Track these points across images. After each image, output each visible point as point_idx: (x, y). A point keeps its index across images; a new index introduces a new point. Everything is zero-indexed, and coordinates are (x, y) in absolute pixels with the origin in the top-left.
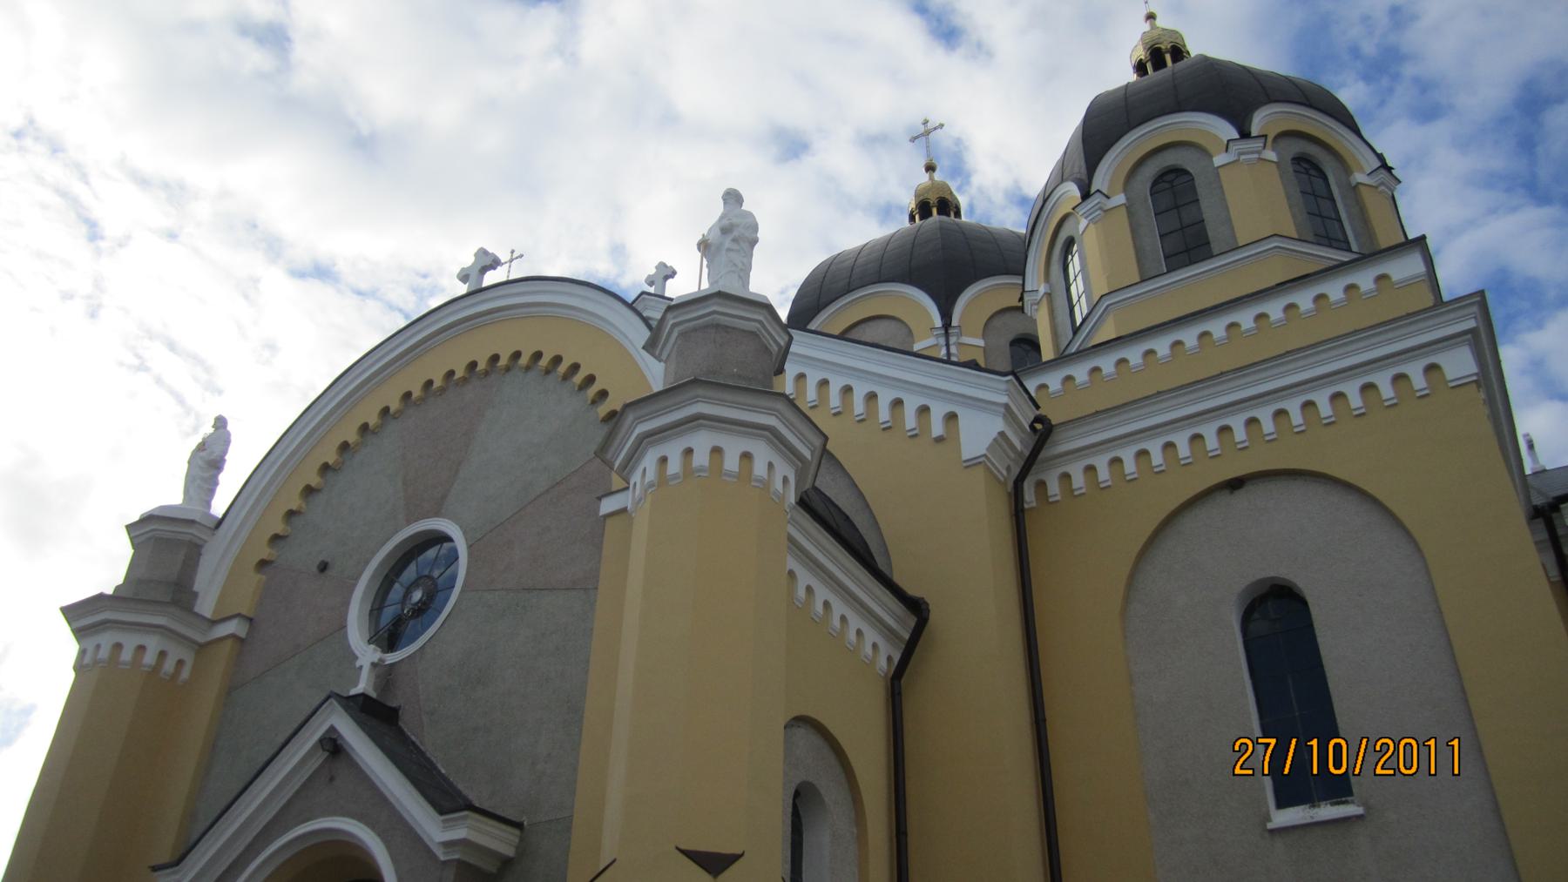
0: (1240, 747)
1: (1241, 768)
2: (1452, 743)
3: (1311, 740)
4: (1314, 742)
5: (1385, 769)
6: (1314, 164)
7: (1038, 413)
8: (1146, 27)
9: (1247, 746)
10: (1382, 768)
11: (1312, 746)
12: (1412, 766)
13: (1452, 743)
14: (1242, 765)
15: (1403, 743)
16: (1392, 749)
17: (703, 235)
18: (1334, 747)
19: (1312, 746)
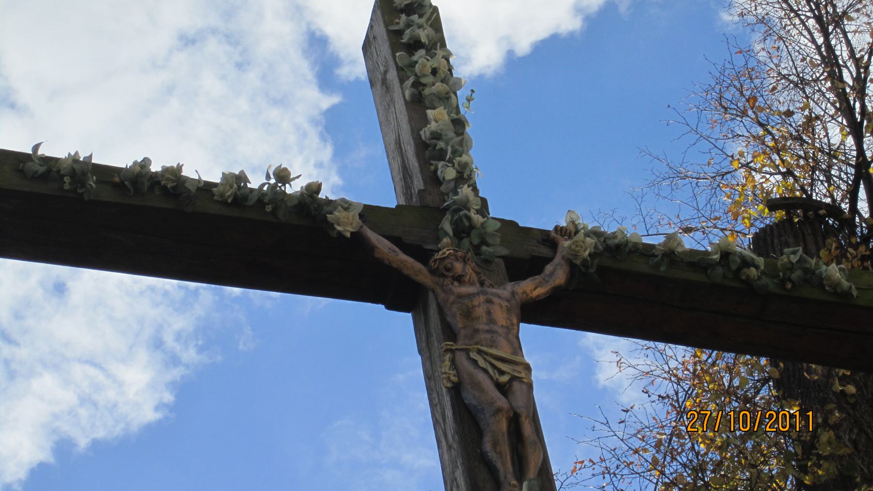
0: (769, 416)
1: (691, 428)
2: (730, 414)
3: (809, 412)
4: (810, 413)
5: (693, 428)
6: (405, 182)
7: (635, 231)
8: (470, 93)
9: (695, 415)
10: (770, 428)
11: (809, 415)
12: (747, 426)
13: (730, 414)
14: (691, 426)
15: (742, 413)
16: (775, 417)
17: (69, 154)
18: (743, 416)
19: (809, 415)
